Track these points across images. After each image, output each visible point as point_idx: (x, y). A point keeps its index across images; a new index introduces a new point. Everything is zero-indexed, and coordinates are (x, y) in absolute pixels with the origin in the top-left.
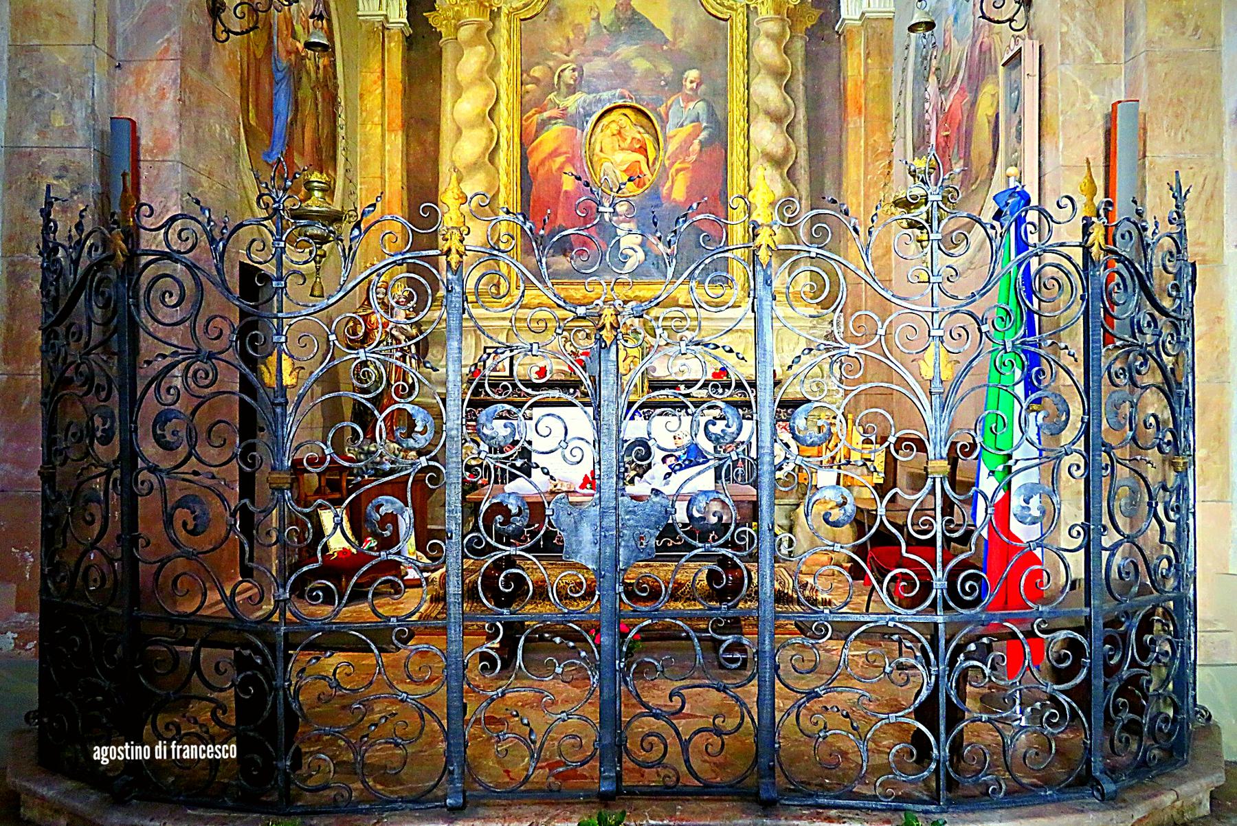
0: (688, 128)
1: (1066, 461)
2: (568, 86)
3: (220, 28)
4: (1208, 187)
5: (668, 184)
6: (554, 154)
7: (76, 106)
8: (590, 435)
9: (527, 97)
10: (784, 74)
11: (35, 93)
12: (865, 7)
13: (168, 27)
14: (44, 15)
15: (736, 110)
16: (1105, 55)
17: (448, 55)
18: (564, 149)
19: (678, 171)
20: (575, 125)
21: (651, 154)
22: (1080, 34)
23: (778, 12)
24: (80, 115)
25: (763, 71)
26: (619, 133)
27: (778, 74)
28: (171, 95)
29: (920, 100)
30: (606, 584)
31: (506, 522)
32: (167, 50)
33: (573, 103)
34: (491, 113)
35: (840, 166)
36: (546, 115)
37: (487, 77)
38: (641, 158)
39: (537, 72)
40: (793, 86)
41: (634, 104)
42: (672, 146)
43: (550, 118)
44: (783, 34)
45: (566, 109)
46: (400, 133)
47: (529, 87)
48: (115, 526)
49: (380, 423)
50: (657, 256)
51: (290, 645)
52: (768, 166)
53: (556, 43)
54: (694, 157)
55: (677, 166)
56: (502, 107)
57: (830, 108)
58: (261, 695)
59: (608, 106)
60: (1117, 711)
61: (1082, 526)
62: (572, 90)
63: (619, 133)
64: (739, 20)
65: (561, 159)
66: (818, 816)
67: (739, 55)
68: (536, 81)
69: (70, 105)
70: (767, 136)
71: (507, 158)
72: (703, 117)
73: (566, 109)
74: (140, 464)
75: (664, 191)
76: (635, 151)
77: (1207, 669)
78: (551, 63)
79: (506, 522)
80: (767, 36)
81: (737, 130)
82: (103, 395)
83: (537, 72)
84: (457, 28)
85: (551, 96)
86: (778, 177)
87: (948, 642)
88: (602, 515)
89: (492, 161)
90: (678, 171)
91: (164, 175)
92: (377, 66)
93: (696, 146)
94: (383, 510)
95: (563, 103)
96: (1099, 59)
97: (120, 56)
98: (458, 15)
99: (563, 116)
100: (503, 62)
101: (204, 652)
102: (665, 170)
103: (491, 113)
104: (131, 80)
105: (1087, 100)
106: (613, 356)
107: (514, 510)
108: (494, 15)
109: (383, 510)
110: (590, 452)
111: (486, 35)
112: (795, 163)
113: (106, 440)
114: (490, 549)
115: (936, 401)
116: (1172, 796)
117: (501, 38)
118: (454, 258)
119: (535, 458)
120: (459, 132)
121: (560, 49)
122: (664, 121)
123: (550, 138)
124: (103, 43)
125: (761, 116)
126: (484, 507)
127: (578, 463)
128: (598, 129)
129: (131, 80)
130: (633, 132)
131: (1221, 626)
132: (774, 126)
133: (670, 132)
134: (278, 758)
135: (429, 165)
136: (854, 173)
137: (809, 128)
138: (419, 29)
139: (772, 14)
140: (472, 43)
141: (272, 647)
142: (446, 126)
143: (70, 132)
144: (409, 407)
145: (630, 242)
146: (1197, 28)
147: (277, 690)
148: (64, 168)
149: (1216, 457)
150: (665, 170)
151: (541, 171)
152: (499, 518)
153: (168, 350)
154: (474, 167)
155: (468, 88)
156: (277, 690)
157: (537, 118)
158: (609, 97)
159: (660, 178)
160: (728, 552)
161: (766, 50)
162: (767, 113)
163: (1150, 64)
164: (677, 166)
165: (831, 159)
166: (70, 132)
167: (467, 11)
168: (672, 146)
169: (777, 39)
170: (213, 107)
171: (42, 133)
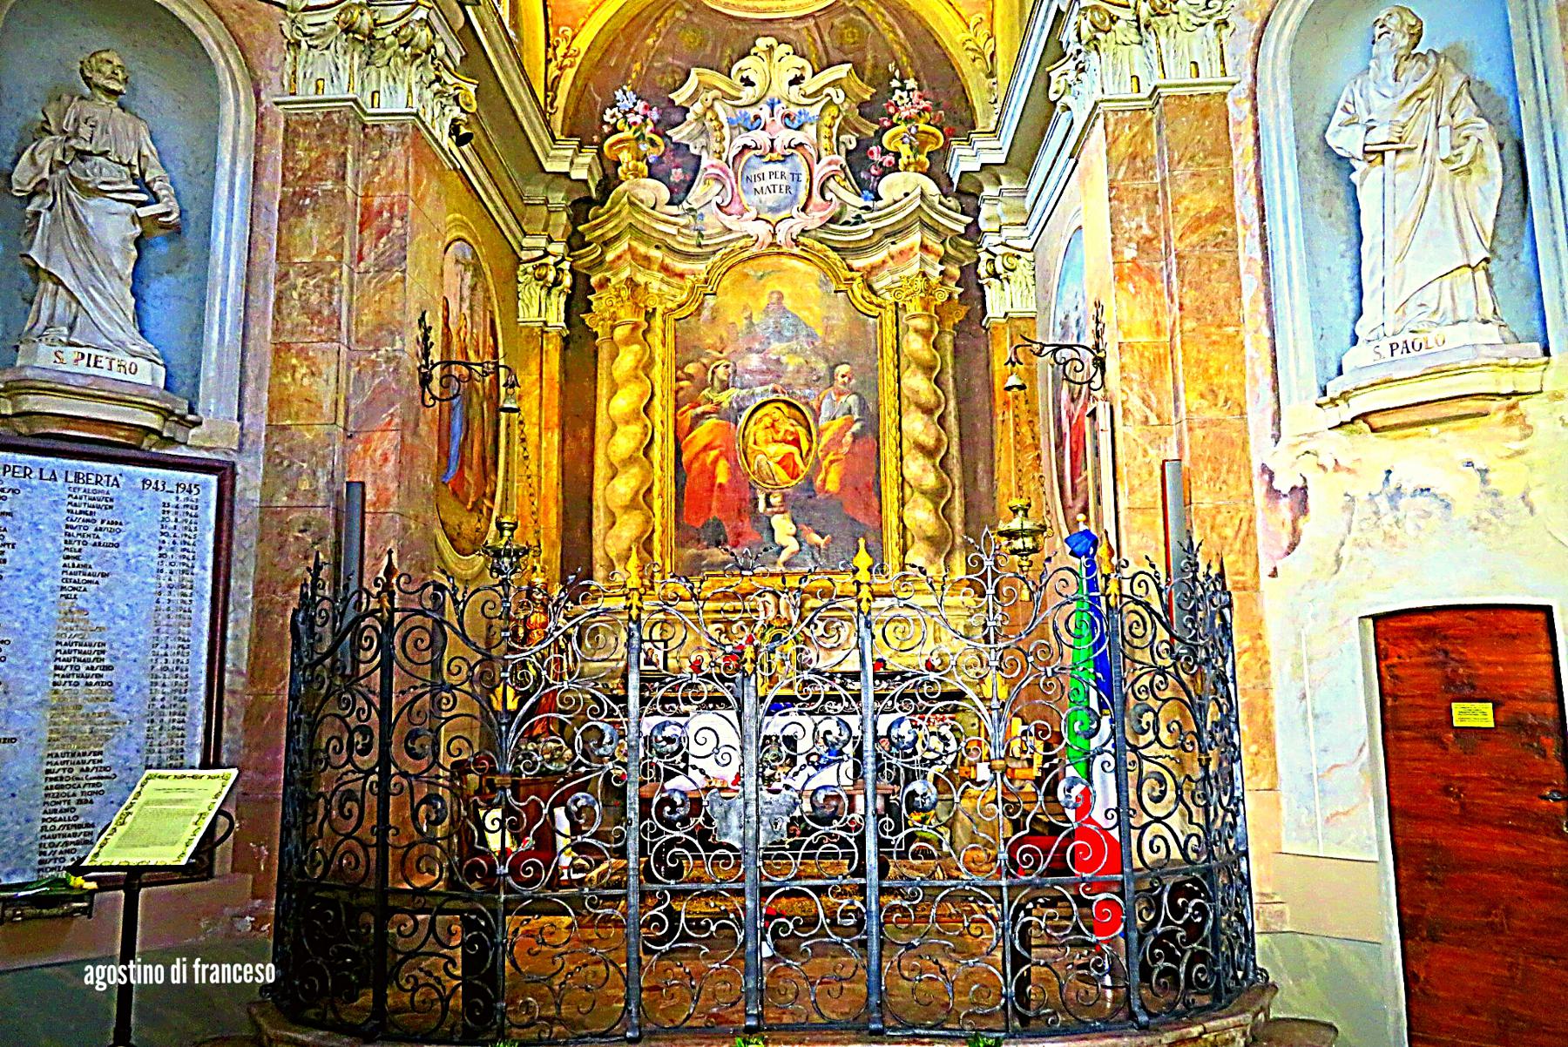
0: (840, 421)
1: (1098, 760)
2: (722, 381)
3: (428, 396)
4: (1244, 527)
5: (821, 476)
6: (708, 447)
7: (319, 474)
8: (737, 744)
9: (681, 394)
10: (932, 369)
11: (286, 463)
12: (1008, 309)
13: (392, 404)
14: (295, 401)
15: (889, 402)
16: (1159, 417)
17: (604, 354)
18: (718, 443)
19: (832, 462)
20: (728, 419)
21: (805, 445)
22: (1139, 402)
23: (926, 309)
24: (323, 480)
25: (913, 366)
26: (773, 426)
27: (928, 369)
28: (392, 458)
29: (1057, 401)
30: (750, 859)
31: (673, 811)
32: (389, 423)
33: (725, 398)
34: (646, 409)
35: (992, 456)
36: (699, 410)
37: (641, 374)
38: (794, 449)
39: (691, 369)
40: (943, 378)
41: (786, 398)
42: (825, 439)
43: (704, 413)
44: (931, 331)
45: (719, 404)
46: (557, 431)
47: (684, 383)
48: (370, 821)
49: (578, 737)
50: (811, 547)
51: (508, 912)
52: (920, 455)
53: (709, 341)
54: (846, 449)
55: (831, 457)
56: (656, 401)
57: (980, 401)
58: (484, 951)
59: (760, 401)
60: (1154, 960)
61: (1117, 810)
62: (725, 387)
63: (773, 426)
64: (889, 316)
65: (713, 453)
66: (915, 1042)
67: (889, 352)
68: (690, 377)
69: (315, 473)
70: (917, 426)
71: (663, 451)
72: (855, 410)
73: (719, 404)
74: (393, 770)
75: (818, 483)
76: (788, 443)
77: (1266, 937)
78: (705, 361)
79: (673, 811)
80: (916, 331)
81: (889, 421)
82: (364, 717)
83: (691, 369)
84: (613, 328)
85: (705, 392)
86: (930, 467)
87: (1010, 904)
88: (746, 805)
89: (646, 454)
90: (832, 462)
91: (385, 522)
92: (534, 367)
93: (848, 438)
94: (580, 803)
95: (717, 398)
96: (1153, 420)
97: (352, 428)
98: (614, 317)
99: (716, 412)
100: (658, 360)
101: (439, 918)
102: (818, 462)
103: (646, 409)
104: (359, 447)
105: (1145, 454)
106: (752, 682)
107: (679, 802)
108: (650, 316)
109: (580, 803)
110: (736, 755)
111: (640, 333)
112: (947, 452)
113: (365, 751)
114: (660, 833)
115: (995, 714)
116: (1200, 1029)
117: (655, 339)
118: (634, 612)
119: (692, 761)
120: (614, 430)
121: (713, 347)
122: (817, 414)
123: (702, 434)
124: (341, 422)
125: (913, 407)
126: (655, 800)
127: (1293, 546)
128: (752, 423)
129: (359, 447)
130: (786, 426)
131: (1277, 899)
132: (925, 417)
133: (823, 423)
134: (497, 1000)
135: (585, 459)
136: (1005, 465)
137: (959, 419)
138: (576, 331)
139: (919, 311)
140: (627, 342)
141: (494, 912)
142: (602, 426)
143: (314, 493)
144: (601, 725)
145: (783, 527)
146: (1226, 401)
147: (496, 946)
148: (307, 523)
149: (1264, 752)
150: (818, 462)
151: (696, 465)
152: (667, 809)
153: (419, 683)
154: (631, 460)
155: (623, 385)
156: (496, 946)
157: (691, 413)
158: (761, 393)
159: (812, 469)
160: (843, 834)
161: (915, 345)
162: (919, 406)
163: (1190, 429)
164: (831, 457)
165: (983, 449)
166: (314, 493)
167: (622, 313)
168: (825, 439)
169: (925, 334)
170: (422, 460)
171: (290, 496)
